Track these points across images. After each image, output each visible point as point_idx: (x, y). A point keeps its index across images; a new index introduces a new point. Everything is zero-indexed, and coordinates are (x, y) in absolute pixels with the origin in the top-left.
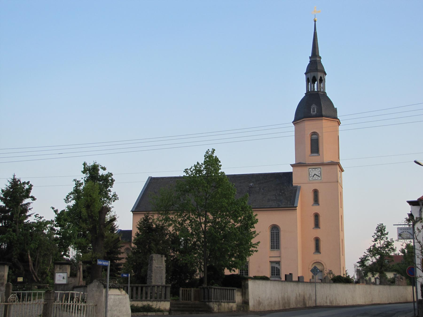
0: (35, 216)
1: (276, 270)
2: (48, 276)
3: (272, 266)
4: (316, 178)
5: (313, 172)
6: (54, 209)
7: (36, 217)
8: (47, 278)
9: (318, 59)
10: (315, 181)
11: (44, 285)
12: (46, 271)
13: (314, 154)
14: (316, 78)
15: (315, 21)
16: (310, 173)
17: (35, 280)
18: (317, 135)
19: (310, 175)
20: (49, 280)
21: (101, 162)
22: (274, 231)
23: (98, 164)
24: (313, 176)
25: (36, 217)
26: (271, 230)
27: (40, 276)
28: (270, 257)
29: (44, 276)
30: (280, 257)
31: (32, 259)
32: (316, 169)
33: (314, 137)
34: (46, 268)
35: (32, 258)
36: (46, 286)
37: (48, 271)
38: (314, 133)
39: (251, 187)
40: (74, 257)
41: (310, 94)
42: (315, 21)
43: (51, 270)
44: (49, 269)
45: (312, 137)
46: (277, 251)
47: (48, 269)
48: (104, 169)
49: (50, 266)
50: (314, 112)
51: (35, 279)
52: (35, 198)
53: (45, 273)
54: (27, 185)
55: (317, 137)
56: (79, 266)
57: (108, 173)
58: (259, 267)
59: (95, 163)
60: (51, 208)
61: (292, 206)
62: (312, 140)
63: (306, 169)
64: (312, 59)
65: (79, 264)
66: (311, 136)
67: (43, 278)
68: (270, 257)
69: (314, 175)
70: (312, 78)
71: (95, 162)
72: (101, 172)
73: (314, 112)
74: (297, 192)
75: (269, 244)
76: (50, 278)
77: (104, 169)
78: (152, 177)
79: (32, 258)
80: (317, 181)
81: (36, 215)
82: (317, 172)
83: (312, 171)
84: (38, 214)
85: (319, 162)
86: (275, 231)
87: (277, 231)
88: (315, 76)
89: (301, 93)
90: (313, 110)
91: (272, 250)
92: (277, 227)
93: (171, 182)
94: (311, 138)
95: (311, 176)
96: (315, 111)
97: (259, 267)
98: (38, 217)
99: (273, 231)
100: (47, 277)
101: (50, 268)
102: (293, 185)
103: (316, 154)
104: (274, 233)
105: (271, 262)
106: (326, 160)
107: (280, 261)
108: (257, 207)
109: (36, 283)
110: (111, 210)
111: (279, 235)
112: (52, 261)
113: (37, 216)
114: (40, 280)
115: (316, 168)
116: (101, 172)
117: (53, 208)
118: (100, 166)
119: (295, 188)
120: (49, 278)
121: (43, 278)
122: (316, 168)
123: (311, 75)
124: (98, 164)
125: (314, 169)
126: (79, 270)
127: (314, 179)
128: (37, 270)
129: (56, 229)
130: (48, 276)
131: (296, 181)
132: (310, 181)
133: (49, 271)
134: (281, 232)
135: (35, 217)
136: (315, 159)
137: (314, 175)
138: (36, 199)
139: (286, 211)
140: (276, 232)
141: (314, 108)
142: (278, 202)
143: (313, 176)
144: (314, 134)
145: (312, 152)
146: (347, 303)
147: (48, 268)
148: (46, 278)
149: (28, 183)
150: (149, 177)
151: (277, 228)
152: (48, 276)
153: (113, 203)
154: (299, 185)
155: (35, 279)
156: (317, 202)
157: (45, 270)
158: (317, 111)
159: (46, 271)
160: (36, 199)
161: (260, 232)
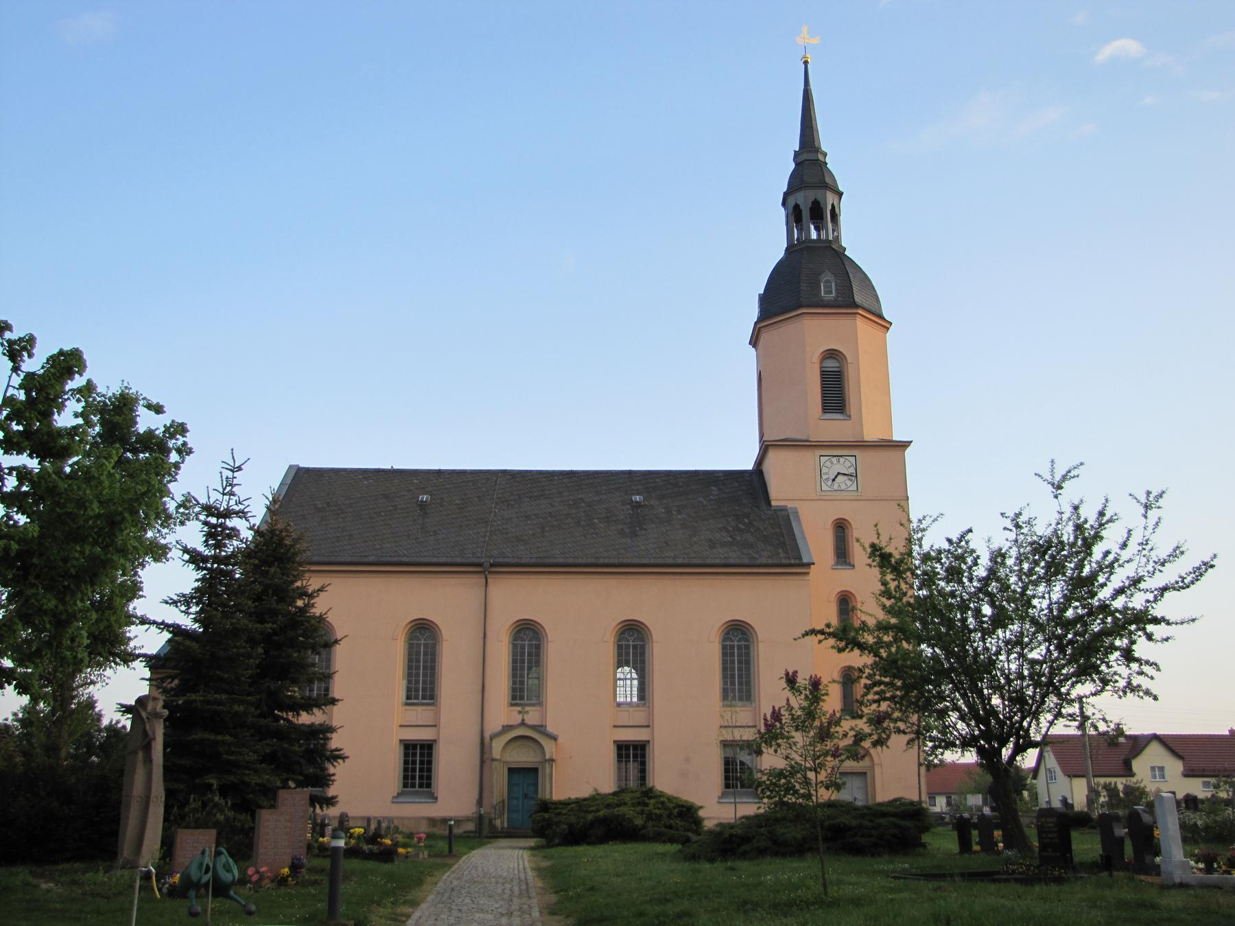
1: (420, 760)
3: (725, 758)
4: (843, 487)
5: (833, 466)
9: (821, 157)
10: (839, 493)
13: (831, 414)
14: (822, 205)
15: (806, 63)
16: (824, 470)
18: (834, 358)
19: (824, 477)
22: (733, 641)
23: (137, 392)
24: (834, 480)
30: (648, 726)
32: (841, 459)
33: (831, 364)
38: (832, 354)
39: (638, 505)
41: (806, 247)
42: (806, 63)
45: (824, 365)
46: (743, 706)
48: (158, 409)
55: (838, 365)
57: (173, 421)
58: (687, 760)
59: (126, 388)
61: (797, 561)
63: (810, 457)
65: (144, 714)
69: (836, 477)
70: (810, 205)
71: (126, 384)
72: (146, 421)
73: (831, 293)
74: (794, 524)
75: (506, 700)
77: (158, 409)
80: (844, 493)
82: (845, 465)
83: (828, 464)
85: (849, 437)
86: (736, 643)
88: (819, 199)
89: (776, 249)
90: (825, 287)
91: (725, 702)
92: (744, 629)
93: (365, 482)
94: (821, 368)
96: (833, 292)
97: (687, 760)
99: (728, 643)
102: (773, 503)
104: (732, 647)
105: (725, 744)
106: (871, 435)
107: (649, 742)
108: (680, 561)
110: (168, 556)
111: (748, 654)
115: (841, 456)
116: (146, 421)
118: (144, 399)
119: (783, 513)
122: (841, 456)
123: (804, 199)
124: (137, 392)
125: (834, 460)
127: (836, 487)
131: (780, 491)
132: (823, 494)
134: (760, 645)
136: (834, 428)
137: (836, 477)
140: (739, 647)
141: (828, 281)
142: (745, 551)
143: (834, 480)
144: (830, 357)
150: (291, 467)
151: (743, 633)
153: (178, 528)
156: (845, 558)
158: (837, 291)
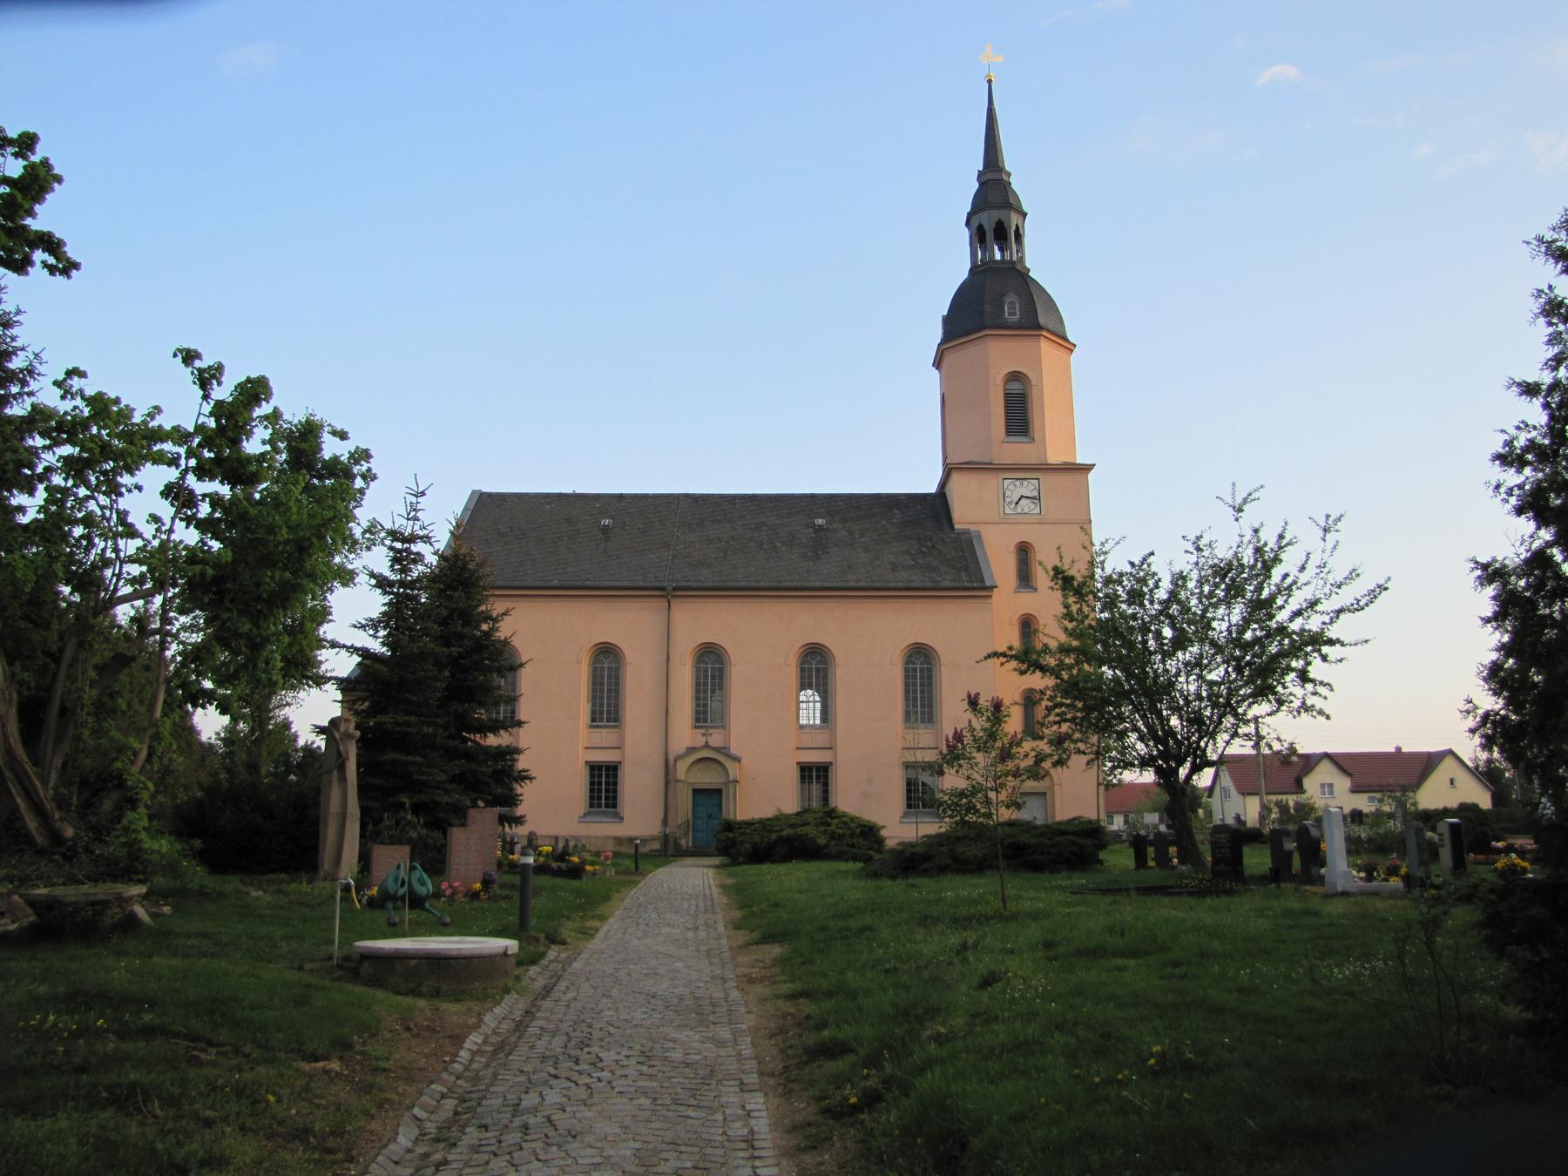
0: (57, 384)
2: (132, 802)
4: (1026, 510)
5: (1016, 489)
6: (198, 364)
7: (63, 397)
8: (125, 822)
9: (1005, 177)
10: (1022, 516)
11: (101, 890)
12: (119, 765)
14: (1006, 226)
15: (990, 82)
17: (28, 835)
19: (1007, 500)
20: (143, 835)
21: (328, 415)
24: (1017, 503)
25: (63, 397)
26: (907, 663)
27: (75, 801)
28: (798, 748)
29: (107, 805)
30: (831, 748)
31: (13, 675)
33: (1015, 387)
34: (121, 749)
35: (17, 667)
36: (122, 901)
37: (135, 769)
38: (1015, 376)
40: (218, 734)
42: (990, 82)
43: (155, 760)
44: (144, 754)
46: (926, 728)
47: (135, 754)
48: (343, 436)
49: (151, 731)
50: (1015, 314)
51: (32, 824)
52: (71, 252)
53: (118, 781)
54: (16, 155)
56: (341, 748)
59: (311, 414)
60: (175, 355)
61: (980, 585)
62: (1008, 396)
64: (984, 178)
65: (337, 735)
66: (1005, 384)
67: (93, 819)
68: (798, 748)
70: (994, 225)
72: (331, 448)
73: (1015, 314)
76: (147, 824)
77: (343, 436)
78: (483, 491)
79: (17, 667)
81: (71, 373)
82: (1028, 488)
83: (1012, 487)
84: (83, 375)
87: (925, 666)
94: (1005, 390)
95: (1011, 502)
98: (81, 392)
99: (911, 666)
100: (130, 815)
101: (150, 747)
102: (956, 526)
103: (1023, 439)
105: (908, 766)
108: (863, 584)
109: (40, 852)
111: (930, 677)
112: (165, 702)
113: (76, 383)
114: (69, 832)
116: (331, 448)
117: (189, 357)
118: (329, 425)
120: (145, 822)
121: (93, 819)
123: (988, 219)
125: (1018, 483)
126: (335, 774)
127: (1019, 510)
128: (58, 762)
129: (198, 492)
130: (132, 802)
131: (963, 513)
133: (140, 772)
135: (60, 392)
136: (1017, 451)
138: (76, 266)
139: (958, 601)
140: (922, 670)
143: (1017, 503)
145: (1010, 431)
146: (1001, 878)
147: (136, 745)
148: (119, 819)
149: (27, 143)
150: (474, 492)
151: (926, 656)
152: (134, 809)
153: (365, 554)
154: (973, 528)
155: (32, 824)
157: (116, 759)
159: (119, 765)
160: (76, 266)
161: (1389, 579)
